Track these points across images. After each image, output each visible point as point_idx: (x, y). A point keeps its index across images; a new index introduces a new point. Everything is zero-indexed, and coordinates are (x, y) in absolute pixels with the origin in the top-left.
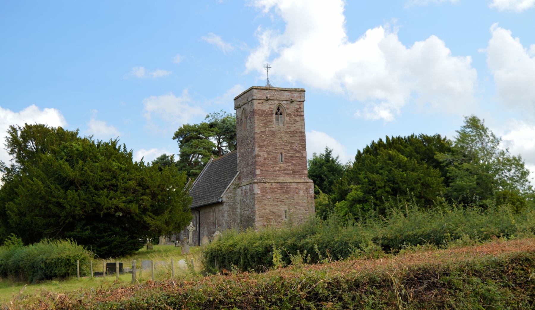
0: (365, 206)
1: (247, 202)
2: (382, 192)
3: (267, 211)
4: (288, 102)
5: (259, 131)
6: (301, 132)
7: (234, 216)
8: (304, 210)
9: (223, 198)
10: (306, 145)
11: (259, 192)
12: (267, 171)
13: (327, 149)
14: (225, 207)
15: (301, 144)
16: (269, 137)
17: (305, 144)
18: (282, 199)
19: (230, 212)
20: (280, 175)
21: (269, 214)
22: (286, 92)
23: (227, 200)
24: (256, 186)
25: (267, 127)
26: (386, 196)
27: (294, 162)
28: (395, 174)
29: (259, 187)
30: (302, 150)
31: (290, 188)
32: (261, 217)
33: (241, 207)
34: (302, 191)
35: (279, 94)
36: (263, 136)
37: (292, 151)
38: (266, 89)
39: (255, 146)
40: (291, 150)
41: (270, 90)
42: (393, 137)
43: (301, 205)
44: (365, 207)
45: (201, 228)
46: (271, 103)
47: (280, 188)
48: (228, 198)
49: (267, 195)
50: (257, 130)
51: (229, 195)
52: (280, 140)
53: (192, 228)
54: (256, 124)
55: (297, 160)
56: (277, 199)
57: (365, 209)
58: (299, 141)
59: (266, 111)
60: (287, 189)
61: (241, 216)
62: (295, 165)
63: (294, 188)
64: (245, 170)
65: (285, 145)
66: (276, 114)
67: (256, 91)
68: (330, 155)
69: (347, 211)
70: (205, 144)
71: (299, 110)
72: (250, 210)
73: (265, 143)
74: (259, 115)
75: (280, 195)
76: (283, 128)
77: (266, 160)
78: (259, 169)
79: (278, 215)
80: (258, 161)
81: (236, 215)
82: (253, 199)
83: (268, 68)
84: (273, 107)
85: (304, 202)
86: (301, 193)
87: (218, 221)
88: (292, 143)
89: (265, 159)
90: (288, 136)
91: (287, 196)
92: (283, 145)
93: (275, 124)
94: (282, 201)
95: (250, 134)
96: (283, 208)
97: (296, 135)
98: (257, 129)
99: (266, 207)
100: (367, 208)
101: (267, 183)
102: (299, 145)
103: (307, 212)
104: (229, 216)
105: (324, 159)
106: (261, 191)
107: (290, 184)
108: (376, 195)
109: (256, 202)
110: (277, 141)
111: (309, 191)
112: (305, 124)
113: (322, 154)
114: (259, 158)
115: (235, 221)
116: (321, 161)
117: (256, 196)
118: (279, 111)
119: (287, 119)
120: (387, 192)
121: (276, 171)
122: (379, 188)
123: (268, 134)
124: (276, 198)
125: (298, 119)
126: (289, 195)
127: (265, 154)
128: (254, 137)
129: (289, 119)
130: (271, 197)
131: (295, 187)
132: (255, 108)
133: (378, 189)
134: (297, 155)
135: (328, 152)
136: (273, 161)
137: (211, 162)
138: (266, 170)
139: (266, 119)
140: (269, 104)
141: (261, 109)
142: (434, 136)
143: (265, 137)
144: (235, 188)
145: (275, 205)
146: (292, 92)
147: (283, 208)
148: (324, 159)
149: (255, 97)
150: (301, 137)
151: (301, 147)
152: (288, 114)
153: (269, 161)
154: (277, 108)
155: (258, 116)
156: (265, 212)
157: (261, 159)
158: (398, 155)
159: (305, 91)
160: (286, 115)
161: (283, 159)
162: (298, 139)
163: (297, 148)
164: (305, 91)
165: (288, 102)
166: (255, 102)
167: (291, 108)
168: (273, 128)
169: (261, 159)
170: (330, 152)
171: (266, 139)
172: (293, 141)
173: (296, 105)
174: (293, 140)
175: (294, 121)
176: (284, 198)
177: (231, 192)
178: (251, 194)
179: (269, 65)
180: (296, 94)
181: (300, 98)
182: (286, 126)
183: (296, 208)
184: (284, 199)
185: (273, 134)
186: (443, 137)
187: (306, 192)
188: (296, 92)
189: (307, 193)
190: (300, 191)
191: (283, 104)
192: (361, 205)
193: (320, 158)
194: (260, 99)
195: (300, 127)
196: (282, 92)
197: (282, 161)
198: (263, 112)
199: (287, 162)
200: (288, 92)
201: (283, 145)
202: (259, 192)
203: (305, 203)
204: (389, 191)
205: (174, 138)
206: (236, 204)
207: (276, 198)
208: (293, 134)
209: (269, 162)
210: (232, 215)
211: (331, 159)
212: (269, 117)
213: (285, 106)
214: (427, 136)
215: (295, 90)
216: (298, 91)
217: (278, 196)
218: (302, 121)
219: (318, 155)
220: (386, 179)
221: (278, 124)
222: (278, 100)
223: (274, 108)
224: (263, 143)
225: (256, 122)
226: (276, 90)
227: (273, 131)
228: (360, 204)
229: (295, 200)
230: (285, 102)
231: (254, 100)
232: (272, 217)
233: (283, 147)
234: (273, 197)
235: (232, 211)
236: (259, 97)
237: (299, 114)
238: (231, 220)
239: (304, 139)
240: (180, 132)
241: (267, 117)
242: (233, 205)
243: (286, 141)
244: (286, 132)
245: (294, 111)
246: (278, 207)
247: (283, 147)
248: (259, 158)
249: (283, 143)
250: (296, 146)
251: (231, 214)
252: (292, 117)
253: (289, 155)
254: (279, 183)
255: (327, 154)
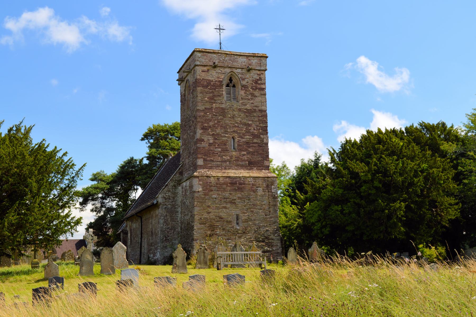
0: (345, 208)
1: (187, 203)
2: (370, 189)
3: (212, 216)
4: (244, 71)
5: (203, 108)
6: (261, 111)
7: (174, 223)
8: (263, 214)
9: (158, 199)
10: (268, 128)
11: (201, 189)
12: (213, 161)
13: (316, 154)
14: (160, 211)
15: (260, 127)
16: (216, 116)
17: (267, 127)
18: (233, 200)
19: (168, 217)
20: (231, 166)
21: (214, 220)
22: (241, 57)
23: (164, 200)
24: (195, 181)
25: (215, 103)
26: (375, 194)
27: (251, 150)
28: (387, 164)
29: (201, 183)
30: (262, 134)
31: (244, 184)
32: (202, 224)
33: (181, 210)
34: (261, 189)
35: (231, 60)
36: (208, 114)
37: (249, 136)
38: (214, 53)
39: (197, 128)
40: (247, 134)
41: (219, 54)
42: (386, 130)
43: (259, 207)
44: (344, 210)
45: (143, 239)
46: (220, 71)
47: (230, 183)
48: (166, 199)
49: (212, 193)
50: (200, 107)
51: (167, 194)
52: (232, 120)
53: (92, 238)
54: (199, 98)
55: (255, 147)
56: (227, 198)
57: (344, 212)
58: (258, 123)
59: (213, 81)
60: (240, 186)
61: (182, 223)
62: (252, 153)
63: (250, 184)
64: (187, 161)
65: (238, 127)
66: (228, 86)
67: (199, 54)
68: (319, 160)
69: (320, 215)
70: (174, 145)
71: (259, 82)
72: (189, 214)
73: (211, 124)
74: (203, 87)
75: (230, 194)
76: (236, 105)
77: (212, 147)
78: (202, 158)
79: (227, 222)
80: (200, 148)
81: (175, 222)
82: (192, 198)
83: (221, 30)
84: (223, 77)
85: (263, 203)
86: (260, 191)
87: (155, 229)
88: (250, 125)
89: (210, 145)
90: (242, 115)
91: (239, 195)
92: (235, 126)
93: (225, 98)
94: (233, 202)
95: (192, 112)
96: (234, 211)
97: (255, 114)
98: (199, 104)
99: (210, 210)
100: (347, 211)
101: (212, 178)
102: (258, 128)
103: (268, 217)
104: (166, 222)
105: (312, 164)
106: (202, 188)
107: (243, 179)
108: (361, 192)
109: (196, 203)
110: (228, 122)
111: (271, 189)
112: (267, 100)
113: (310, 160)
114: (202, 144)
115: (175, 230)
116: (309, 166)
117: (196, 195)
118: (231, 83)
119: (242, 93)
120: (376, 188)
121: (225, 161)
122: (365, 182)
123: (215, 112)
124: (225, 198)
125: (257, 93)
126: (243, 194)
127: (210, 139)
128: (196, 116)
129: (245, 93)
130: (218, 196)
131: (251, 183)
132: (198, 77)
133: (363, 184)
134: (255, 141)
135: (317, 157)
136: (221, 148)
137: (169, 160)
138: (211, 160)
139: (212, 92)
140: (216, 73)
141: (206, 78)
142: (438, 124)
143: (210, 116)
144: (175, 186)
145: (223, 207)
146: (250, 58)
147: (233, 212)
148: (312, 164)
149: (198, 63)
150: (262, 116)
151: (261, 131)
152: (244, 87)
153: (216, 148)
154: (229, 78)
155: (202, 88)
156: (208, 217)
157: (204, 145)
158: (391, 138)
159: (267, 57)
160: (240, 87)
161: (236, 145)
162: (256, 119)
163: (255, 131)
164: (267, 57)
165: (244, 71)
166: (199, 69)
167: (247, 79)
168: (223, 103)
169: (204, 145)
170: (319, 157)
171: (212, 118)
172: (250, 123)
173: (254, 75)
174: (250, 121)
175: (252, 96)
176: (235, 198)
177: (169, 191)
178: (191, 193)
179: (223, 27)
180: (255, 61)
181: (261, 66)
182: (241, 102)
183: (252, 212)
184: (235, 200)
185: (223, 112)
186: (449, 126)
187: (267, 191)
188: (255, 58)
189: (269, 192)
190: (259, 189)
191: (237, 72)
192: (340, 206)
193: (308, 164)
194: (205, 66)
195: (260, 104)
196: (236, 57)
197: (234, 149)
198: (209, 82)
199: (240, 150)
200: (244, 57)
201: (235, 126)
202: (201, 189)
203: (265, 205)
204: (379, 187)
205: (143, 139)
206: (177, 206)
207: (225, 198)
208: (249, 112)
209: (216, 150)
210: (170, 221)
211: (320, 165)
212: (217, 90)
213: (240, 76)
214: (429, 124)
215: (254, 56)
216: (258, 56)
217: (227, 194)
218: (262, 96)
219: (306, 161)
220: (374, 170)
221: (230, 100)
222: (229, 67)
223: (224, 78)
224: (208, 123)
225: (199, 95)
226: (227, 54)
227: (222, 109)
228: (338, 206)
229: (252, 200)
230: (239, 71)
231: (197, 67)
232: (218, 224)
233: (235, 129)
234: (221, 196)
235: (171, 217)
236: (203, 63)
237: (259, 86)
238: (168, 228)
239: (265, 119)
240: (149, 132)
241: (215, 89)
242: (172, 208)
243: (240, 121)
244: (240, 110)
245: (251, 82)
246: (227, 210)
247: (235, 129)
248: (202, 144)
249: (237, 125)
250: (254, 129)
251: (169, 220)
252: (249, 91)
253: (244, 140)
254: (229, 177)
255: (316, 159)
